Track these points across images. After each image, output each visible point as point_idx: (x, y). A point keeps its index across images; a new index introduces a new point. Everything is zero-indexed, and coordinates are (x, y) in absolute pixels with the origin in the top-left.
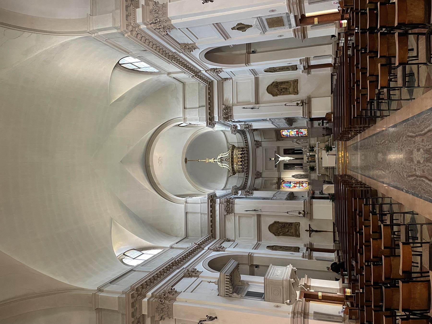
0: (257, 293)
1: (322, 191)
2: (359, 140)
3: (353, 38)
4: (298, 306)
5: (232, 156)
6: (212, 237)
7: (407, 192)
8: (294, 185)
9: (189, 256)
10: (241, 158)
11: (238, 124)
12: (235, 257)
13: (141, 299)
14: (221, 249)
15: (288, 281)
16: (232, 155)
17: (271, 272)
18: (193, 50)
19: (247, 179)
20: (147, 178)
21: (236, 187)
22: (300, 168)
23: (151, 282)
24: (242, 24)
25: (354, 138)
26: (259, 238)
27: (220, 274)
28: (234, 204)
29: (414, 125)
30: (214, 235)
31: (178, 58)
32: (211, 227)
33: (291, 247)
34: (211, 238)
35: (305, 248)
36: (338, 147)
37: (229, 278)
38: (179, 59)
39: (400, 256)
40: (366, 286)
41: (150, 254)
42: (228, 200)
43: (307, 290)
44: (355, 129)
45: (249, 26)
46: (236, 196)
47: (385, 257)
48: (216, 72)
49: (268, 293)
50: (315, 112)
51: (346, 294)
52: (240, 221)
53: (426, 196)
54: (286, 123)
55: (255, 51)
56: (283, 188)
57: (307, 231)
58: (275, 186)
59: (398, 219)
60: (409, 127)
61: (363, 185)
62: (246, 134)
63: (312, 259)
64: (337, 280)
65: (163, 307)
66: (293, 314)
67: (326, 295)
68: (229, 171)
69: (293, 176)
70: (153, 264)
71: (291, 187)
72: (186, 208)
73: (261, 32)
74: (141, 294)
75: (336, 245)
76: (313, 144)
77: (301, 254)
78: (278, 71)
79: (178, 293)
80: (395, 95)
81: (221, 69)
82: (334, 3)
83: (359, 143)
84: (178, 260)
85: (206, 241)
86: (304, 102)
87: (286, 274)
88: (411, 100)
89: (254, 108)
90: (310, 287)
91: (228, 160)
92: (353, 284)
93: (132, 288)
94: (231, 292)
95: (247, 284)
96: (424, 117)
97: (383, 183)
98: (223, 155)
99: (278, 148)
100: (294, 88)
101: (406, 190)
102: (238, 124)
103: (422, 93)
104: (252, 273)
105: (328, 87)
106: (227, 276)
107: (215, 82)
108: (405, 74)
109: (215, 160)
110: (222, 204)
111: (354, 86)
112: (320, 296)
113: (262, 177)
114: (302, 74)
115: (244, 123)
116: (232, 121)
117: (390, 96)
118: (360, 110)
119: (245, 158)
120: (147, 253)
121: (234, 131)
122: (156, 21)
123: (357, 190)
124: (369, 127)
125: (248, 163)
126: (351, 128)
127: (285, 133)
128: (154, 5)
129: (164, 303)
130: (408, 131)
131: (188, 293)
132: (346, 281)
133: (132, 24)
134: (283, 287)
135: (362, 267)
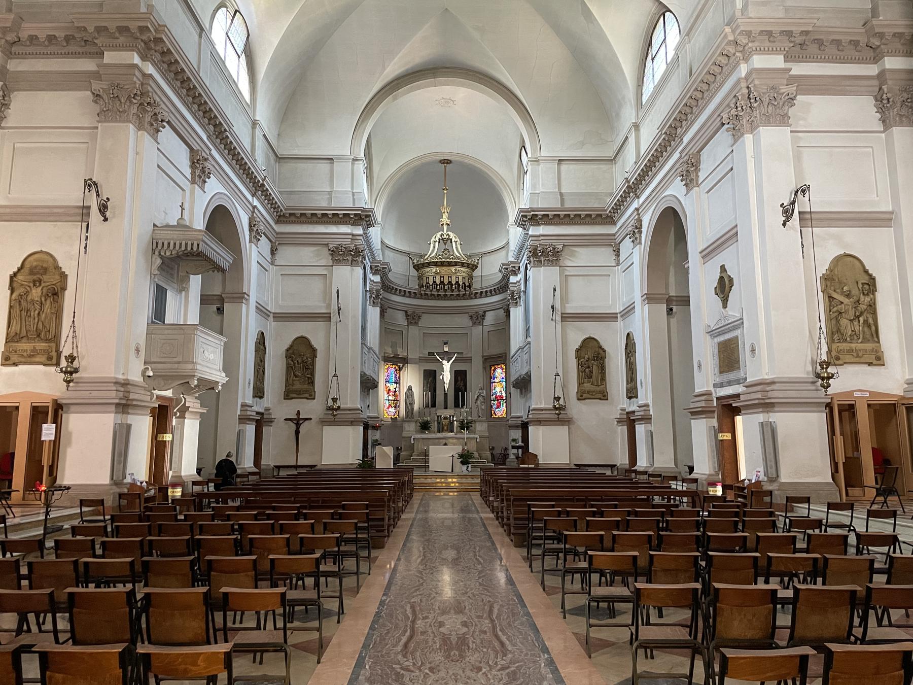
0: (163, 311)
1: (380, 444)
2: (483, 515)
3: (685, 507)
4: (142, 392)
5: (454, 264)
6: (280, 216)
7: (382, 603)
8: (392, 389)
9: (238, 163)
10: (450, 283)
11: (520, 276)
12: (238, 263)
13: (138, 49)
14: (254, 233)
15: (193, 374)
16: (456, 264)
17: (210, 339)
18: (684, 182)
19: (404, 294)
20: (407, 70)
21: (387, 270)
22: (427, 402)
23: (176, 73)
24: (732, 286)
25: (486, 506)
26: (280, 317)
27: (200, 231)
28: (351, 265)
29: (513, 617)
30: (285, 220)
31: (669, 148)
32: (301, 214)
33: (263, 382)
34: (279, 214)
35: (262, 411)
36: (468, 477)
37: (192, 249)
38: (666, 151)
39: (256, 587)
40: (191, 526)
41: (238, 73)
42: (359, 252)
43: (175, 411)
44: (504, 508)
45: (725, 301)
46: (368, 270)
47: (255, 561)
48: (634, 232)
49: (166, 332)
50: (541, 432)
51: (170, 487)
52: (316, 277)
53: (375, 637)
54: (520, 376)
55: (672, 314)
56: (386, 367)
57: (298, 413)
58: (389, 351)
59: (327, 586)
60: (509, 608)
61: (394, 521)
62: (500, 293)
63: (239, 423)
64: (199, 471)
65: (122, 101)
66: (123, 382)
67: (167, 449)
68: (422, 256)
69: (410, 389)
70: (216, 78)
71: (388, 384)
72: (342, 158)
73: (712, 327)
74: (150, 49)
75: (270, 469)
76: (475, 428)
77: (249, 400)
78: (628, 360)
79: (156, 135)
80: (572, 583)
81: (640, 243)
82: (759, 472)
83: (477, 516)
84: (227, 137)
85: (270, 202)
86: (562, 412)
87: (208, 370)
88: (562, 612)
89: (553, 311)
90: (183, 417)
91: (446, 254)
92: (194, 501)
93: (161, 28)
94: (162, 253)
95: (183, 288)
96: (530, 635)
97: (399, 559)
98: (456, 245)
99: (469, 360)
100: (591, 392)
101: (385, 601)
102: (520, 276)
103: (575, 631)
104: (205, 300)
105: (589, 458)
106: (198, 245)
107: (612, 230)
108: (613, 602)
109: (445, 227)
110: (352, 239)
111: (592, 506)
112: (163, 437)
113: (408, 326)
114: (618, 408)
115: (522, 289)
116: (528, 265)
117: (569, 572)
118: (545, 518)
119: (450, 290)
120: (241, 66)
121: (507, 269)
122: (752, 101)
123: (384, 510)
124: (509, 534)
125: (439, 297)
126: (508, 500)
127: (499, 373)
128: (788, 97)
129: (131, 102)
130: (502, 606)
131: (156, 157)
132: (197, 489)
133: (750, 45)
134: (179, 363)
135: (229, 518)
